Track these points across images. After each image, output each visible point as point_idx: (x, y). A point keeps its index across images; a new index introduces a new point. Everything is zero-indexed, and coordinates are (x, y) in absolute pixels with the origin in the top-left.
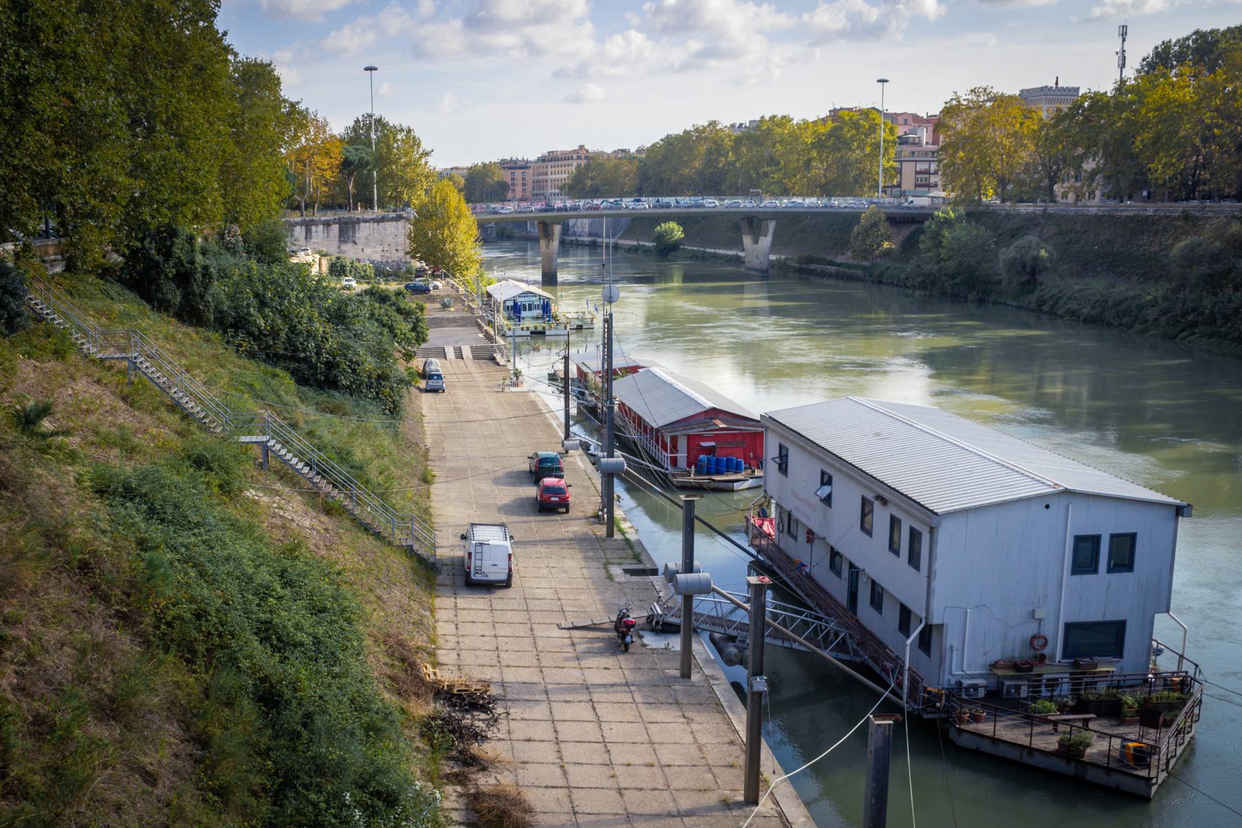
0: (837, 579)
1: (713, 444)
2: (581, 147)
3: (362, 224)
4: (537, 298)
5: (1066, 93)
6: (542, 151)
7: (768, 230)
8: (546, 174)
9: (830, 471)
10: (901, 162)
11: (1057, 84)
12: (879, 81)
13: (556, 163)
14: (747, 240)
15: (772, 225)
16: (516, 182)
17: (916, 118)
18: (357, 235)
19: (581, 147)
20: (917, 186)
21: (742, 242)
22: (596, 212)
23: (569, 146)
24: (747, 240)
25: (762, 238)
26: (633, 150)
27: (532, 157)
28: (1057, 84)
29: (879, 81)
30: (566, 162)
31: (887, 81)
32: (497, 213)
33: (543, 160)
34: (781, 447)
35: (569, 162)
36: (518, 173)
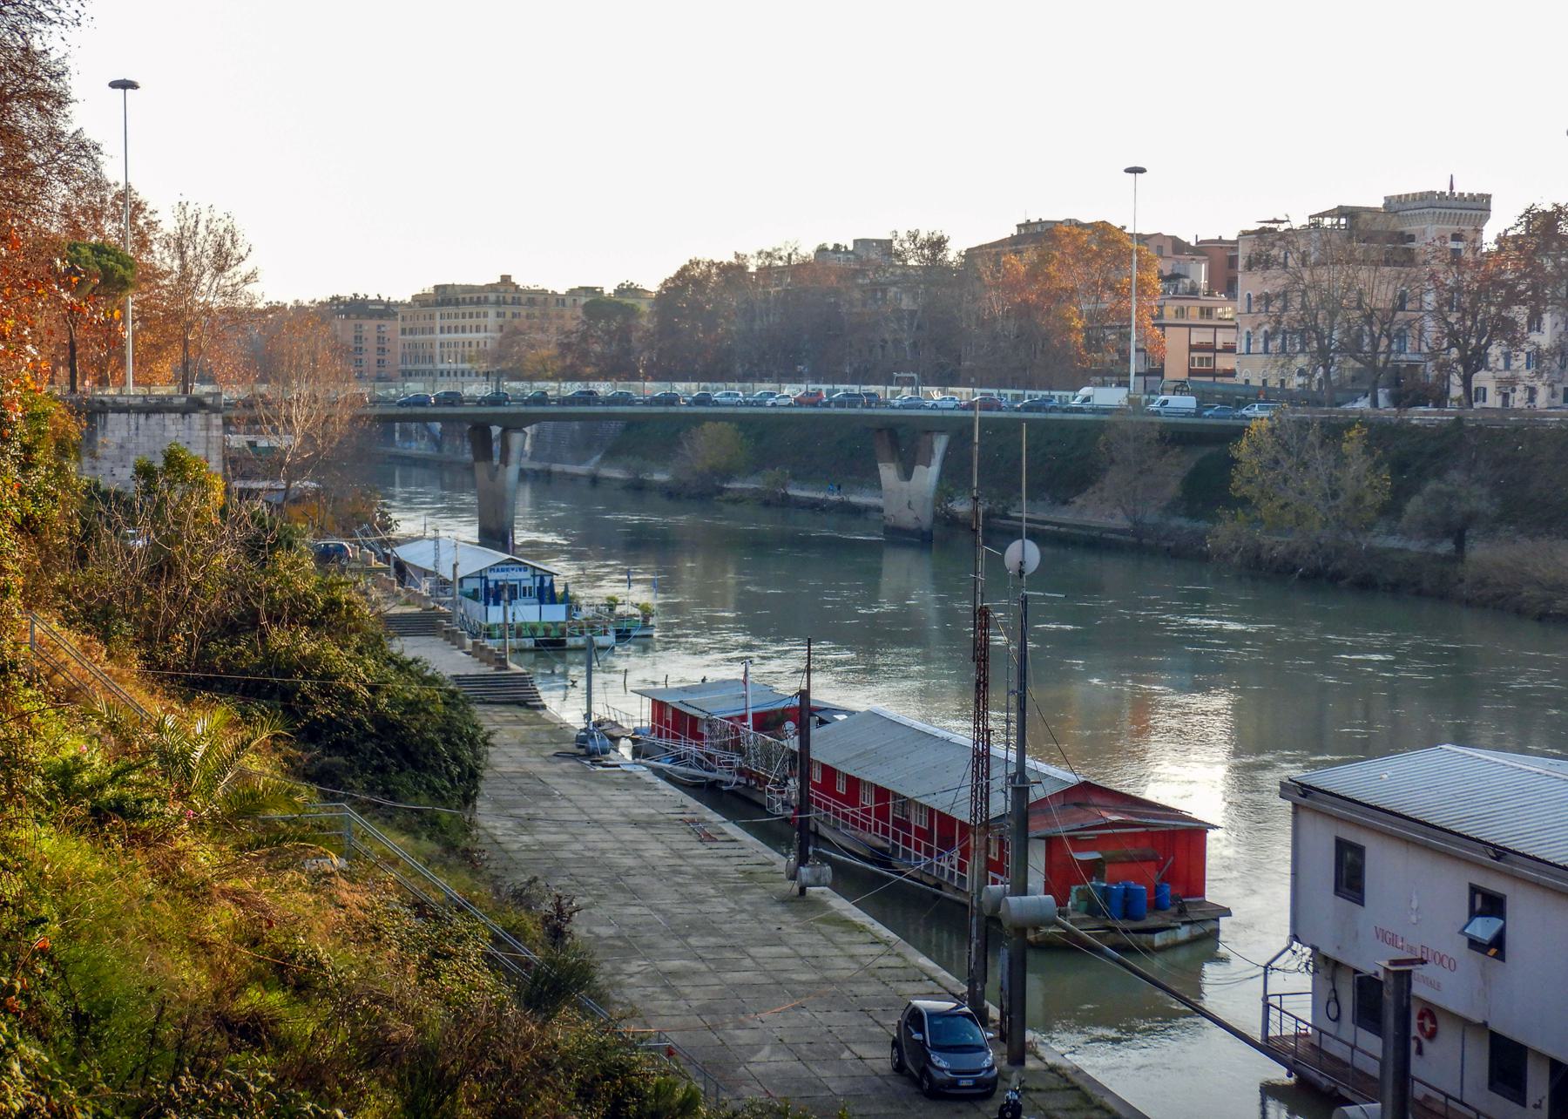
0: (1514, 1107)
1: (1095, 855)
2: (506, 279)
3: (111, 416)
4: (527, 575)
5: (1466, 204)
6: (425, 285)
7: (932, 451)
8: (432, 331)
9: (1495, 885)
10: (1163, 326)
11: (1452, 188)
12: (114, 85)
13: (451, 310)
14: (888, 473)
15: (940, 444)
16: (365, 345)
17: (1178, 246)
18: (100, 439)
19: (506, 279)
20: (1192, 373)
21: (878, 477)
22: (419, 410)
23: (483, 275)
24: (888, 473)
25: (919, 470)
26: (609, 290)
27: (401, 292)
28: (1452, 188)
29: (114, 85)
30: (474, 309)
31: (1142, 171)
32: (879, 403)
33: (420, 300)
34: (1342, 846)
35: (481, 309)
36: (369, 326)
